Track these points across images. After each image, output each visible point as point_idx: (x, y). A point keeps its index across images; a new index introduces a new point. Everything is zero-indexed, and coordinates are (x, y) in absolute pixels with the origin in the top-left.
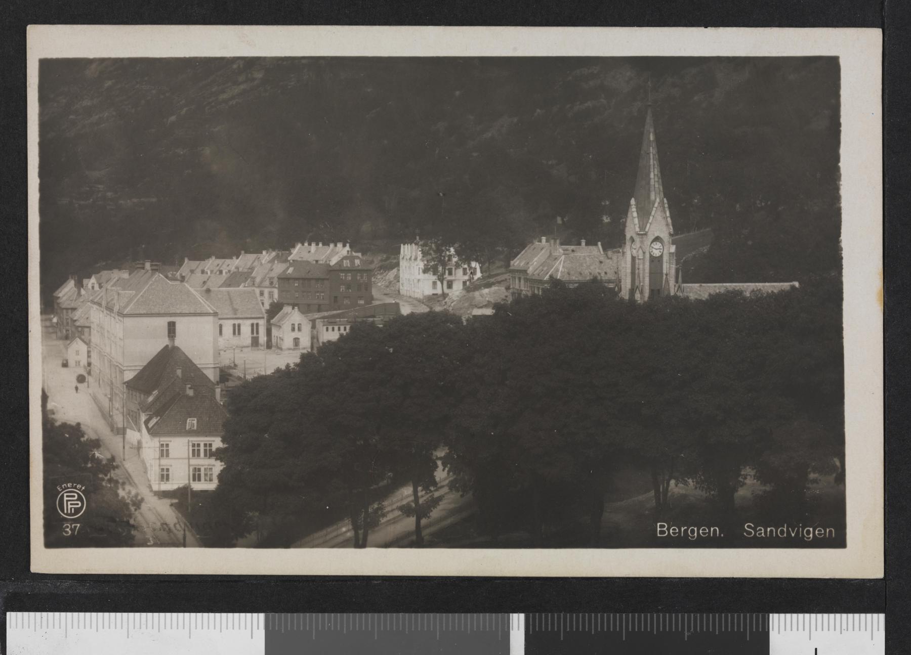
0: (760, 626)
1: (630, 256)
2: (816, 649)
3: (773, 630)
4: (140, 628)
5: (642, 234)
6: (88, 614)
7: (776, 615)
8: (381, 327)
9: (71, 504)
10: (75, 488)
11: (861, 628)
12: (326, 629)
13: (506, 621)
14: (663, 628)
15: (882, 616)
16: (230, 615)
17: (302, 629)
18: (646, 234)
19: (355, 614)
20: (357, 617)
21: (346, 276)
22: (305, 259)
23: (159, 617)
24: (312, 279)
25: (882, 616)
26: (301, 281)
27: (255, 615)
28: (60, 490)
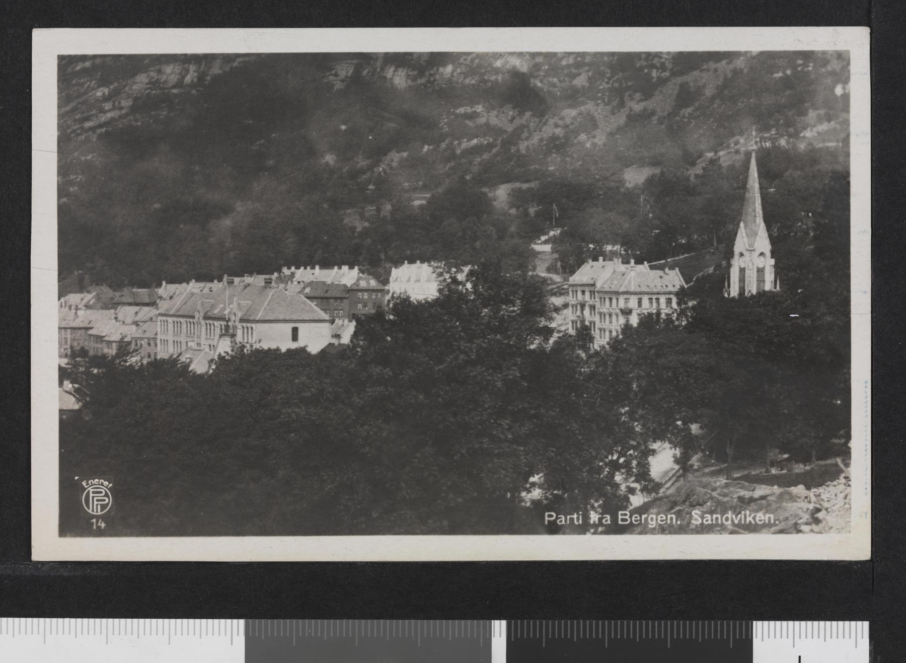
0: (744, 634)
1: (738, 268)
2: (800, 657)
3: (756, 638)
4: (119, 634)
5: (751, 250)
6: (135, 620)
7: (759, 623)
9: (98, 500)
10: (102, 484)
12: (307, 635)
14: (527, 635)
15: (866, 624)
16: (185, 621)
18: (754, 250)
20: (425, 623)
21: (363, 295)
22: (318, 280)
23: (64, 622)
24: (331, 298)
25: (866, 624)
26: (319, 300)
27: (235, 621)
28: (86, 487)
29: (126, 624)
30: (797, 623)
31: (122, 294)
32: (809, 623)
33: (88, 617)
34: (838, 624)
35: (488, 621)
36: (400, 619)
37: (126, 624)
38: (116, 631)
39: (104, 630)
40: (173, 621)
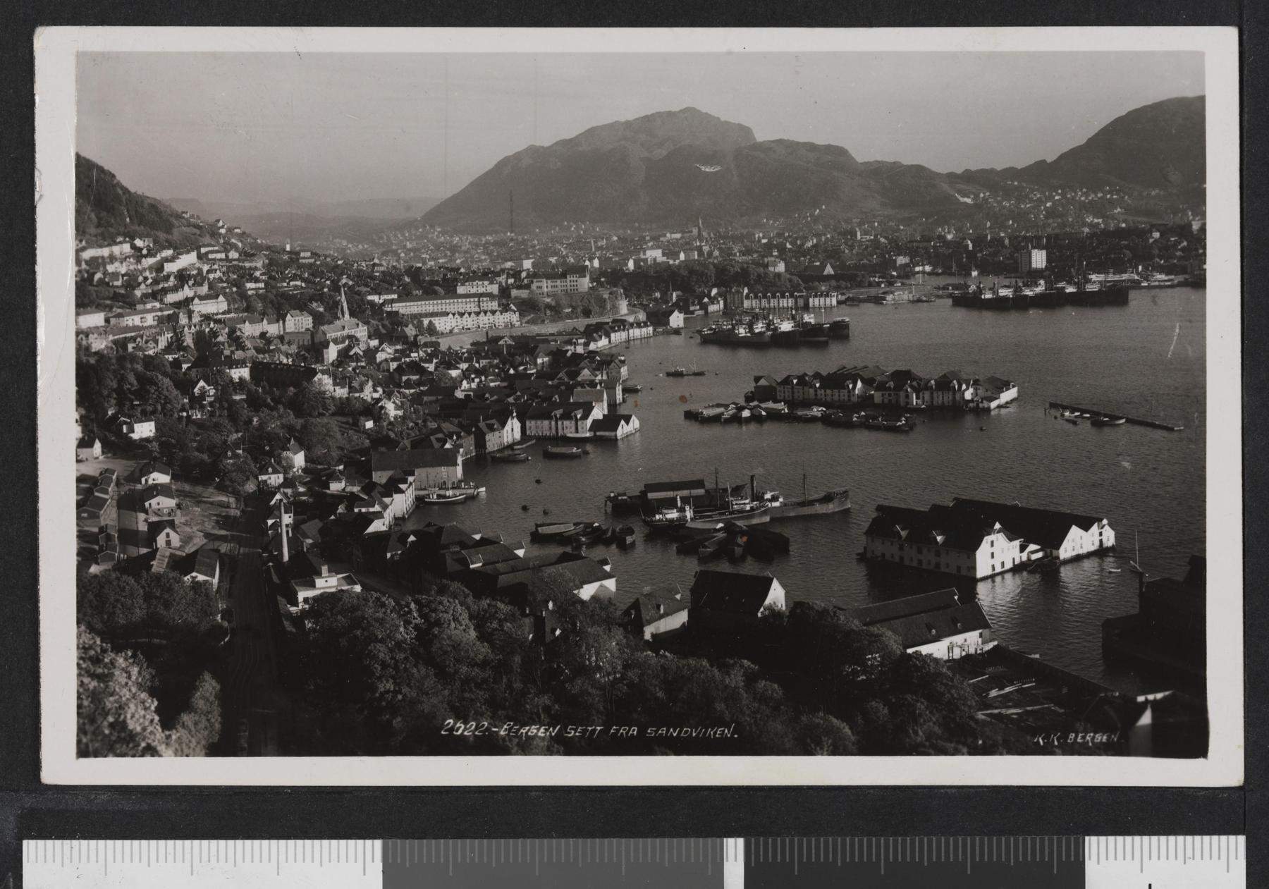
3: (1090, 859)
7: (1094, 839)
15: (1242, 839)
23: (132, 846)
25: (1242, 839)
27: (369, 842)
29: (123, 847)
30: (1146, 838)
31: (555, 284)
32: (1120, 839)
33: (166, 838)
35: (718, 839)
37: (123, 847)
38: (205, 858)
39: (188, 857)
40: (257, 842)
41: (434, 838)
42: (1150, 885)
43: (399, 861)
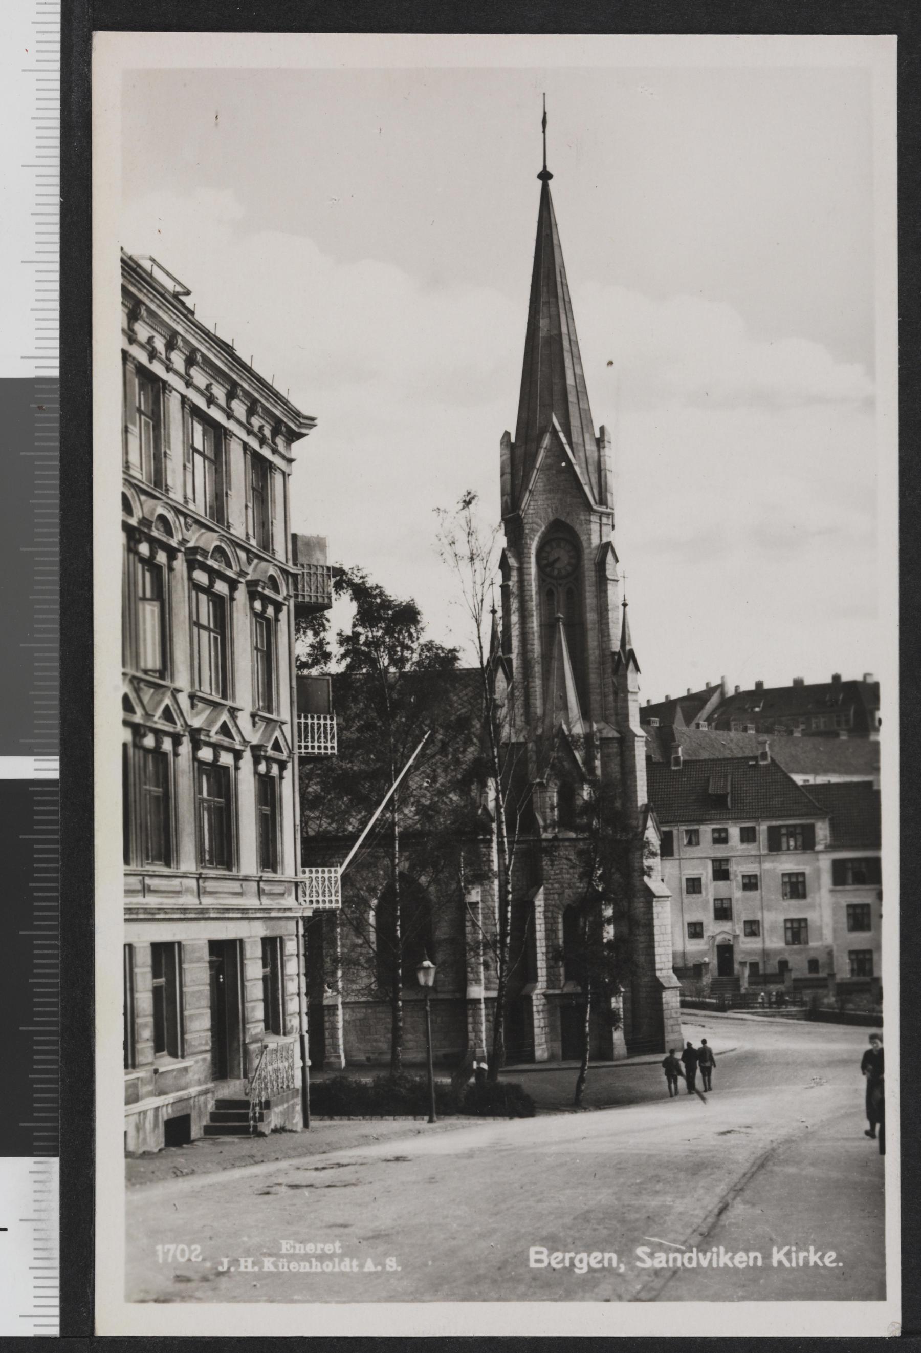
8: (447, 1085)
11: (39, 245)
13: (49, 751)
14: (39, 801)
15: (55, 1331)
17: (36, 664)
19: (59, 564)
25: (55, 1331)
27: (57, 363)
34: (55, 367)
36: (61, 500)
41: (61, 416)
42: (5, 1229)
43: (36, 731)
